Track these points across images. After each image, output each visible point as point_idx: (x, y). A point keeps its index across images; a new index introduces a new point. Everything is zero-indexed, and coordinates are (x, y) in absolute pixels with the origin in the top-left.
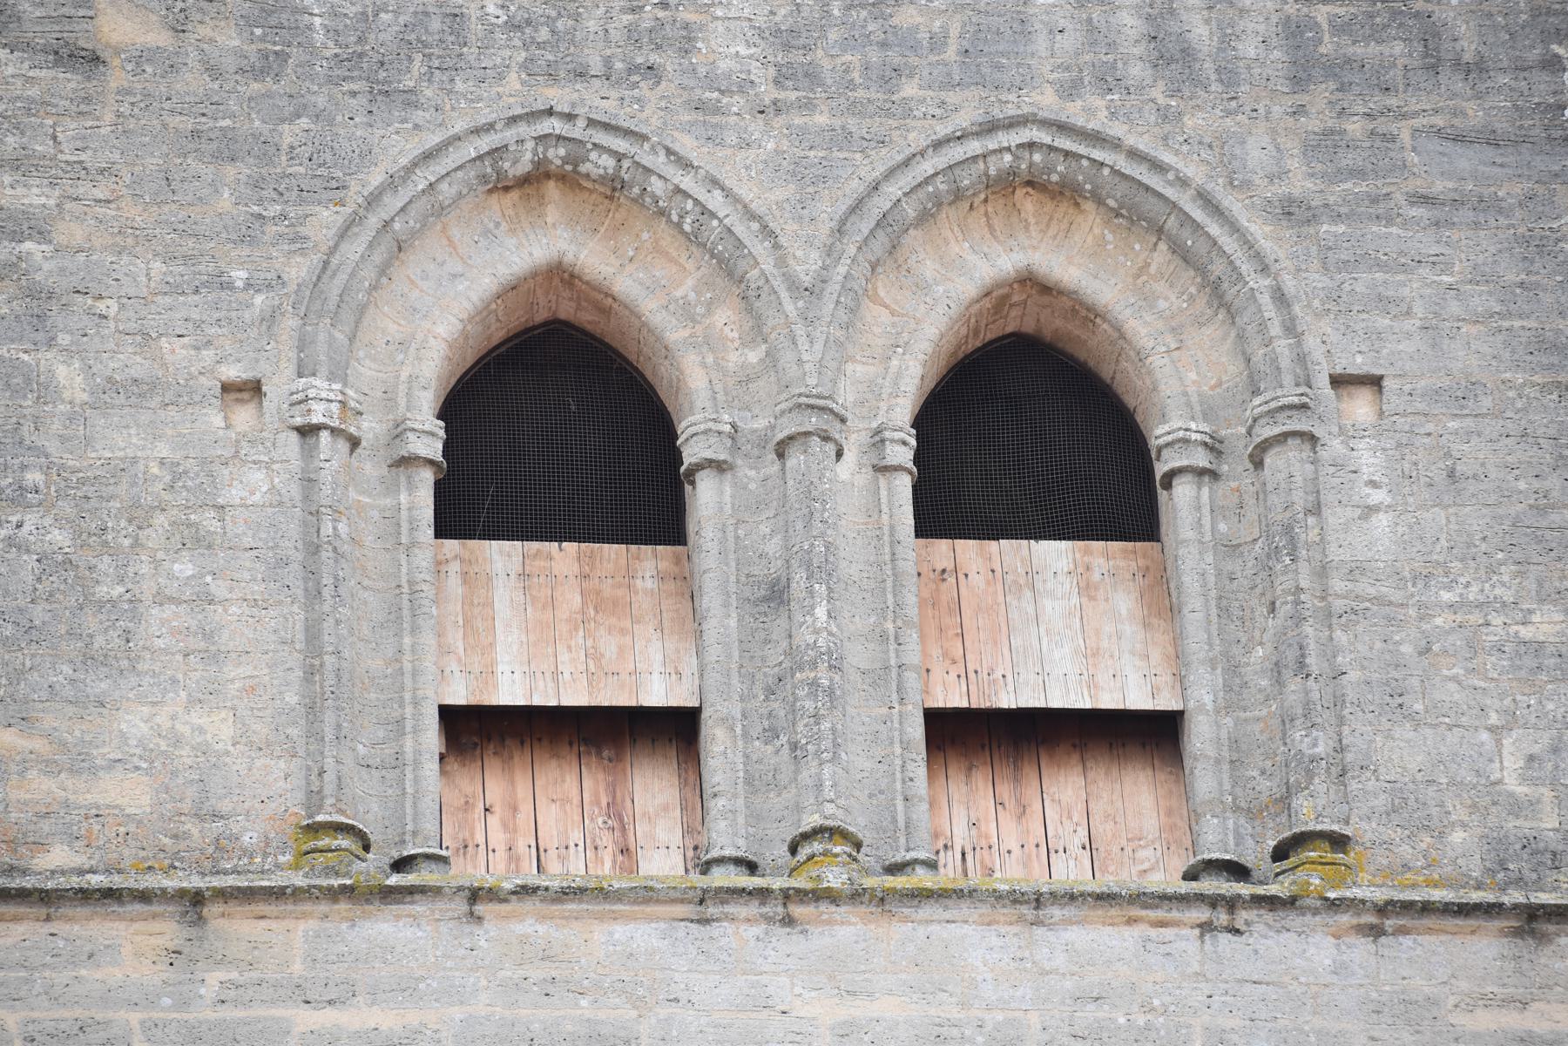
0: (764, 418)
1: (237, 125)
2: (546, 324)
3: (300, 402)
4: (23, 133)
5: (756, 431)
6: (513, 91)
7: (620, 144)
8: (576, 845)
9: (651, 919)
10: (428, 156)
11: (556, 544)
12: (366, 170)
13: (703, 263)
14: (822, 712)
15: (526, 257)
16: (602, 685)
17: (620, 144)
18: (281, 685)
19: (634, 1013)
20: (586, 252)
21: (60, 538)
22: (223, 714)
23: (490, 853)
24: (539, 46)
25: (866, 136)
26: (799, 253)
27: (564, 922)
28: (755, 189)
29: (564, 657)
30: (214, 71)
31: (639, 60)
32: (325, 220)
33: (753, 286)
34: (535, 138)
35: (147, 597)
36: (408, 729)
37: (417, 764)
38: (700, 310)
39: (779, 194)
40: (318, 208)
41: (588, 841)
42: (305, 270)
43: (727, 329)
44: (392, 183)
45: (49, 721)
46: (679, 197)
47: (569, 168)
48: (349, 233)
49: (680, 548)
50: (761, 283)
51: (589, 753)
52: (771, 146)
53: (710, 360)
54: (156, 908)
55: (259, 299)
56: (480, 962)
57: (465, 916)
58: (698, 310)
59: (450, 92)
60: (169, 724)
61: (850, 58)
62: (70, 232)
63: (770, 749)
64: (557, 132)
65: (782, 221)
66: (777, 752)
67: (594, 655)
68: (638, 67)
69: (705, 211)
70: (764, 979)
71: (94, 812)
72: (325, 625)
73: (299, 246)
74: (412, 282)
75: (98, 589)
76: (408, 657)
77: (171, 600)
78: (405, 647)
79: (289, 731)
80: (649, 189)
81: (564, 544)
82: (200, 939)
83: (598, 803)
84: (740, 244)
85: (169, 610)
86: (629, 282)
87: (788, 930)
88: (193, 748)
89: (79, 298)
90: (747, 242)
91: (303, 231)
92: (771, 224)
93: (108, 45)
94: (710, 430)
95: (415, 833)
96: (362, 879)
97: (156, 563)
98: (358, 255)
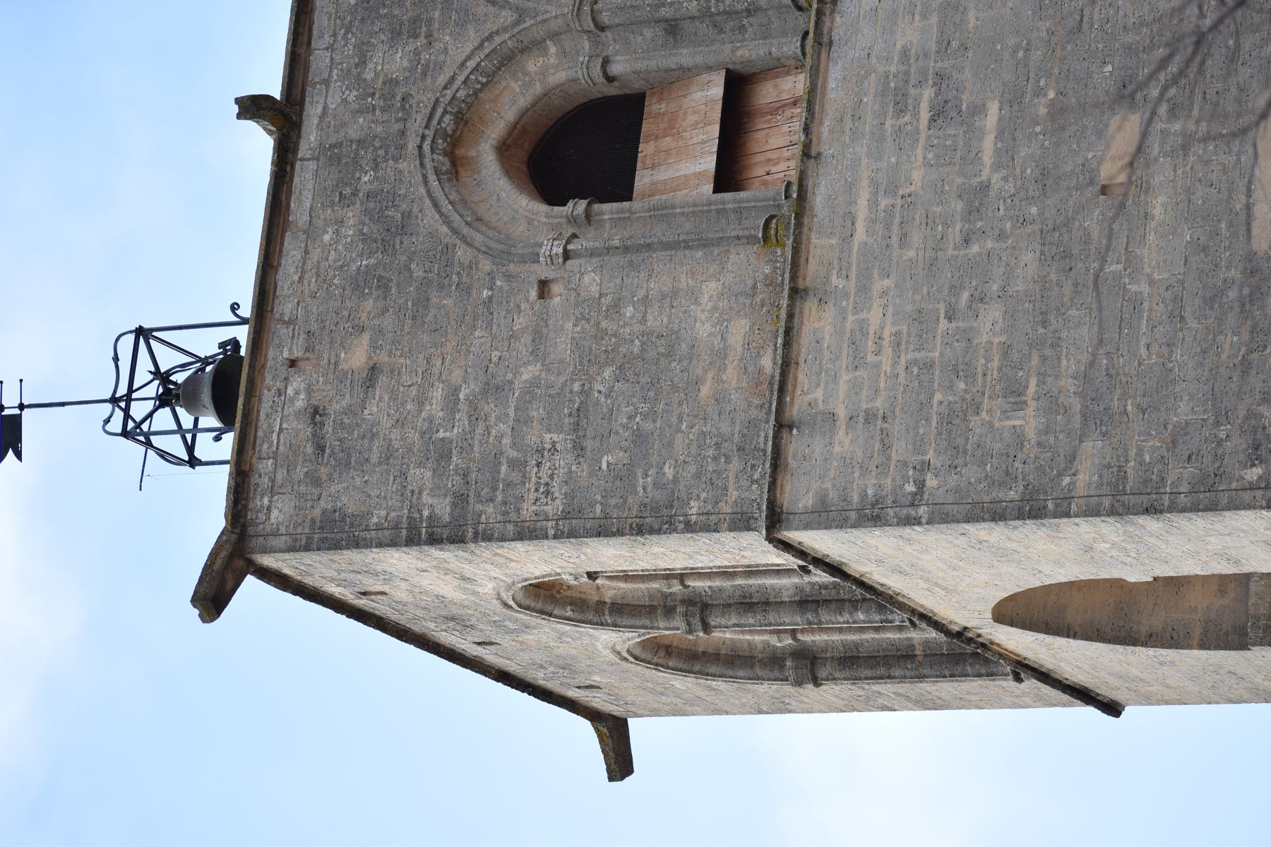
2: (529, 168)
3: (551, 259)
4: (406, 401)
6: (407, 166)
7: (439, 111)
9: (827, 70)
10: (436, 206)
17: (439, 111)
19: (873, 75)
21: (607, 373)
22: (704, 287)
24: (387, 153)
26: (502, 21)
29: (695, 140)
30: (384, 311)
31: (399, 105)
32: (462, 254)
34: (432, 153)
35: (642, 328)
36: (722, 207)
37: (740, 201)
38: (527, 79)
39: (471, 32)
43: (538, 65)
44: (447, 221)
45: (699, 371)
46: (469, 82)
47: (449, 140)
50: (515, 39)
52: (447, 38)
53: (552, 71)
54: (797, 311)
55: (499, 283)
59: (405, 196)
60: (706, 313)
62: (457, 376)
63: (750, 29)
66: (751, 25)
67: (695, 126)
68: (402, 105)
69: (476, 69)
70: (862, 12)
71: (746, 346)
75: (635, 352)
76: (686, 210)
77: (644, 316)
83: (770, 120)
84: (494, 50)
85: (649, 317)
86: (510, 113)
88: (719, 301)
89: (490, 370)
91: (467, 263)
93: (367, 363)
95: (775, 200)
97: (625, 324)
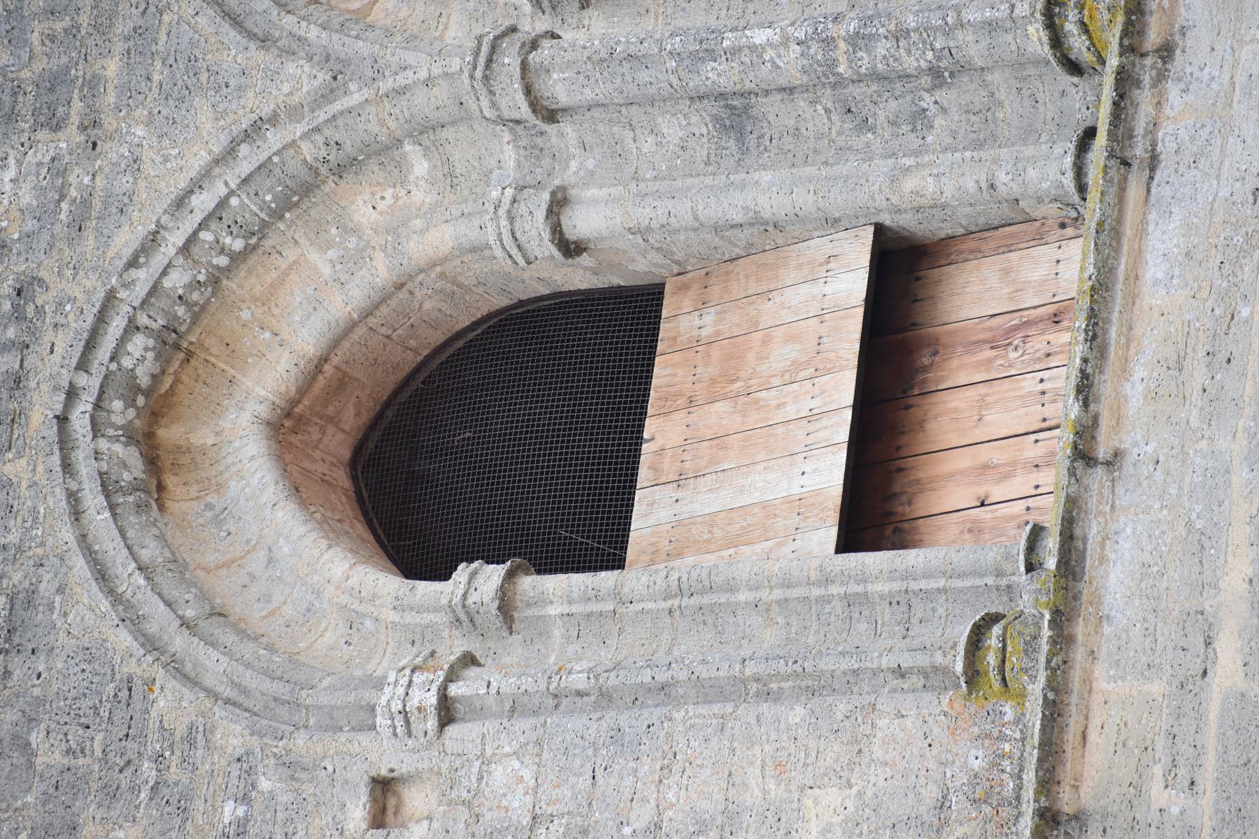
0: (502, 151)
1: (29, 824)
2: (354, 478)
3: (407, 722)
5: (519, 163)
7: (116, 326)
8: (1042, 381)
9: (1142, 231)
10: (102, 575)
11: (644, 446)
12: (110, 653)
13: (289, 234)
14: (892, 27)
15: (256, 464)
16: (832, 356)
17: (116, 326)
18: (778, 730)
20: (258, 389)
22: (808, 802)
23: (1040, 491)
25: (141, 9)
26: (286, 88)
27: (1133, 345)
28: (196, 148)
29: (791, 411)
33: (323, 153)
34: (95, 437)
37: (908, 575)
40: (154, 714)
41: (1038, 367)
42: (233, 726)
43: (381, 206)
44: (132, 619)
46: (195, 250)
48: (193, 675)
49: (668, 289)
50: (319, 139)
51: (924, 382)
52: (140, 130)
53: (418, 223)
55: (265, 784)
56: (1174, 452)
57: (1109, 471)
58: (351, 246)
61: (36, 34)
63: (939, 122)
64: (89, 407)
65: (241, 112)
66: (944, 110)
67: (791, 375)
68: (16, 308)
69: (215, 215)
72: (705, 675)
73: (200, 736)
74: (272, 614)
76: (764, 595)
78: (751, 599)
79: (840, 716)
80: (180, 292)
81: (646, 435)
82: (1105, 816)
83: (990, 361)
84: (264, 167)
87: (1178, 52)
90: (263, 157)
91: (181, 730)
92: (244, 126)
94: (509, 212)
95: (999, 574)
96: (1044, 599)
98: (222, 658)
